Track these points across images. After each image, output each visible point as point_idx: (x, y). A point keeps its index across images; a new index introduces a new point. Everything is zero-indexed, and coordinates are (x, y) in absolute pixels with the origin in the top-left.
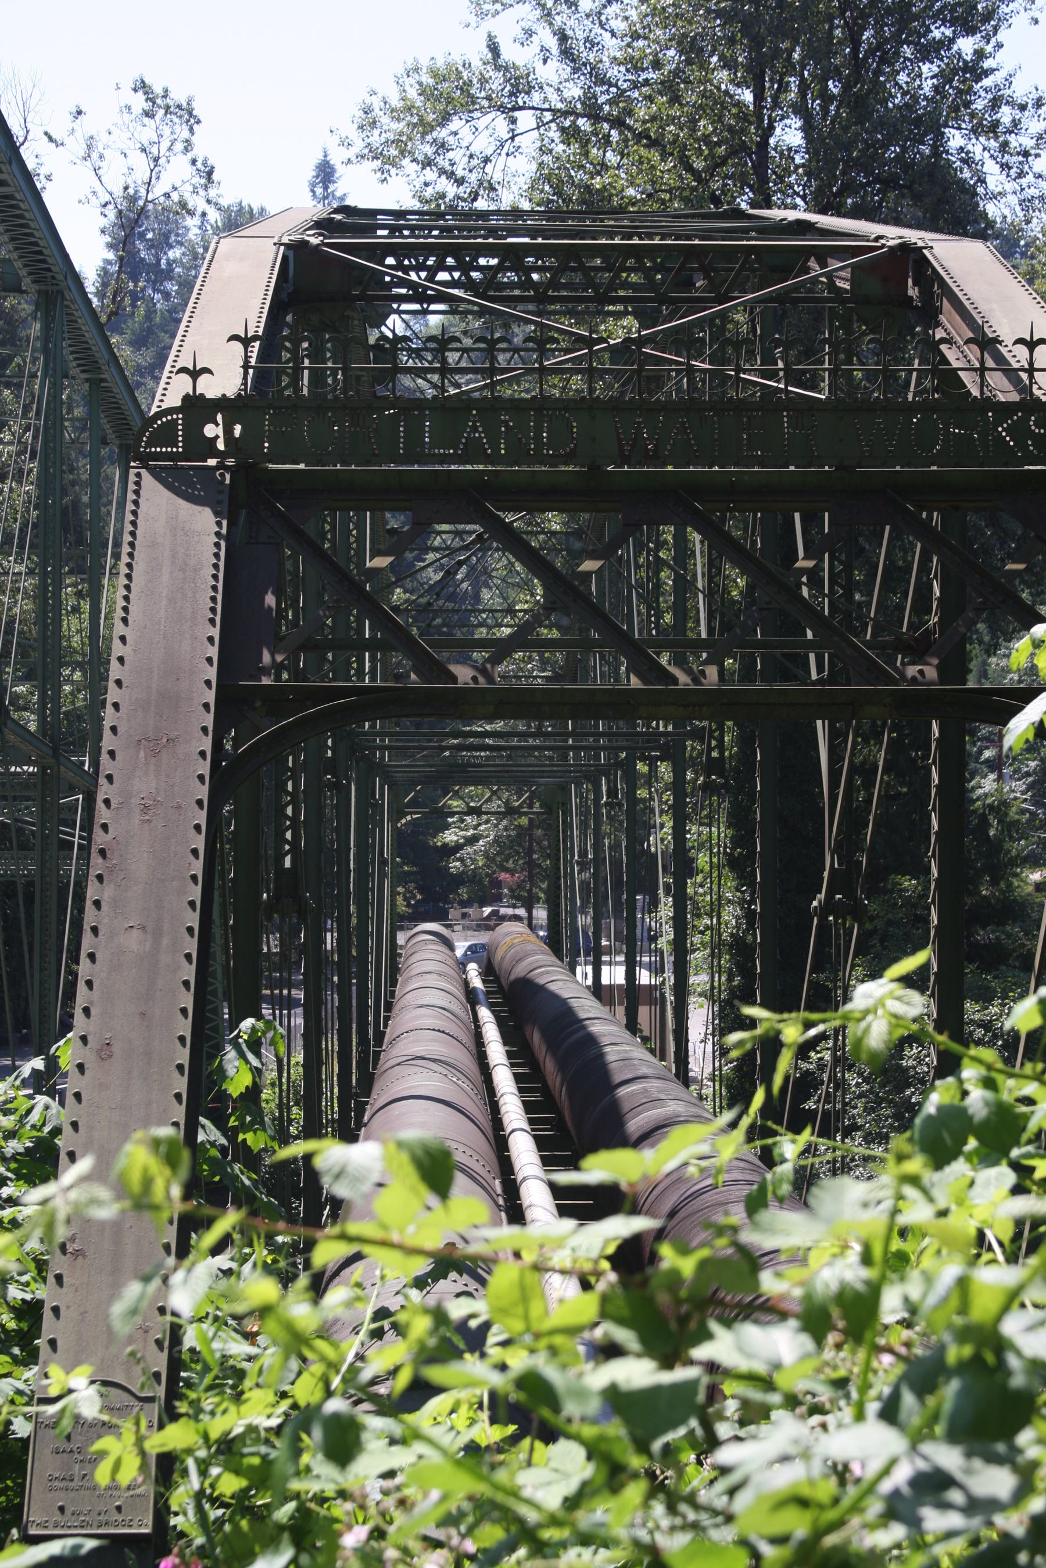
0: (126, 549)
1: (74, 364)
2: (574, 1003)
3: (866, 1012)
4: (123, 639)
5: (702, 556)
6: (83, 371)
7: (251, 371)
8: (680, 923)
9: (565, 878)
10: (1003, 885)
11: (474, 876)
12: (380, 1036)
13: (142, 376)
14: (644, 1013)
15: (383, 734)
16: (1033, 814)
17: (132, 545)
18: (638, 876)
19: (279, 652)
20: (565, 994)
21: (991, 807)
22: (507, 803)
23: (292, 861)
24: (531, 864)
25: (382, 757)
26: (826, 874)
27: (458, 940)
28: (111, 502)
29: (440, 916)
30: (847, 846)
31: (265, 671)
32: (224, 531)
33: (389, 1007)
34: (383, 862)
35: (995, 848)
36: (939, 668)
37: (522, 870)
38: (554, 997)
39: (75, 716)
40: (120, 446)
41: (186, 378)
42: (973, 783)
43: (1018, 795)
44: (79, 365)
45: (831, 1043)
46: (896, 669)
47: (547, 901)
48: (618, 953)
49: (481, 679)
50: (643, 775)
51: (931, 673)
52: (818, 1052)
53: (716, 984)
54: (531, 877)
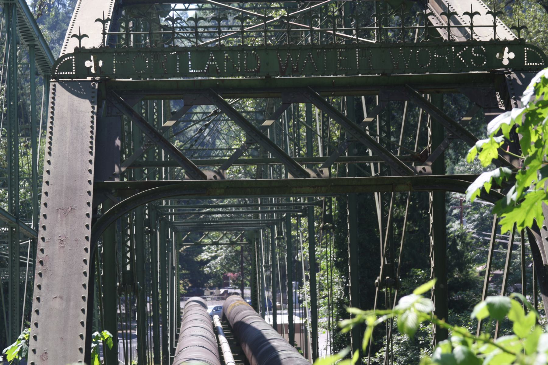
0: (49, 125)
1: (22, 37)
2: (264, 332)
3: (405, 310)
4: (49, 162)
5: (320, 121)
6: (26, 41)
7: (106, 36)
8: (313, 293)
9: (259, 274)
10: (464, 273)
11: (216, 275)
12: (173, 351)
13: (54, 44)
14: (297, 337)
15: (171, 207)
16: (478, 239)
17: (52, 118)
18: (294, 273)
19: (122, 166)
20: (260, 328)
21: (458, 236)
22: (230, 239)
23: (131, 268)
24: (242, 268)
25: (171, 219)
26: (381, 267)
27: (209, 305)
28: (41, 103)
29: (201, 294)
30: (391, 254)
31: (116, 176)
32: (95, 111)
33: (177, 337)
34: (173, 268)
35: (460, 254)
36: (432, 167)
37: (238, 271)
38: (255, 329)
39: (26, 204)
40: (45, 76)
41: (76, 40)
42: (449, 225)
43: (470, 230)
44: (24, 38)
45: (386, 348)
46: (412, 168)
47: (250, 286)
48: (284, 309)
49: (218, 177)
50: (294, 225)
51: (429, 169)
52: (380, 353)
53: (331, 322)
54: (242, 274)
